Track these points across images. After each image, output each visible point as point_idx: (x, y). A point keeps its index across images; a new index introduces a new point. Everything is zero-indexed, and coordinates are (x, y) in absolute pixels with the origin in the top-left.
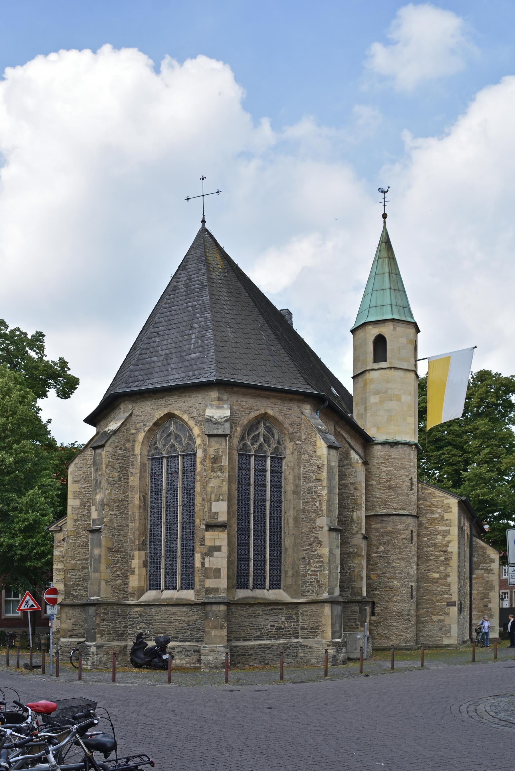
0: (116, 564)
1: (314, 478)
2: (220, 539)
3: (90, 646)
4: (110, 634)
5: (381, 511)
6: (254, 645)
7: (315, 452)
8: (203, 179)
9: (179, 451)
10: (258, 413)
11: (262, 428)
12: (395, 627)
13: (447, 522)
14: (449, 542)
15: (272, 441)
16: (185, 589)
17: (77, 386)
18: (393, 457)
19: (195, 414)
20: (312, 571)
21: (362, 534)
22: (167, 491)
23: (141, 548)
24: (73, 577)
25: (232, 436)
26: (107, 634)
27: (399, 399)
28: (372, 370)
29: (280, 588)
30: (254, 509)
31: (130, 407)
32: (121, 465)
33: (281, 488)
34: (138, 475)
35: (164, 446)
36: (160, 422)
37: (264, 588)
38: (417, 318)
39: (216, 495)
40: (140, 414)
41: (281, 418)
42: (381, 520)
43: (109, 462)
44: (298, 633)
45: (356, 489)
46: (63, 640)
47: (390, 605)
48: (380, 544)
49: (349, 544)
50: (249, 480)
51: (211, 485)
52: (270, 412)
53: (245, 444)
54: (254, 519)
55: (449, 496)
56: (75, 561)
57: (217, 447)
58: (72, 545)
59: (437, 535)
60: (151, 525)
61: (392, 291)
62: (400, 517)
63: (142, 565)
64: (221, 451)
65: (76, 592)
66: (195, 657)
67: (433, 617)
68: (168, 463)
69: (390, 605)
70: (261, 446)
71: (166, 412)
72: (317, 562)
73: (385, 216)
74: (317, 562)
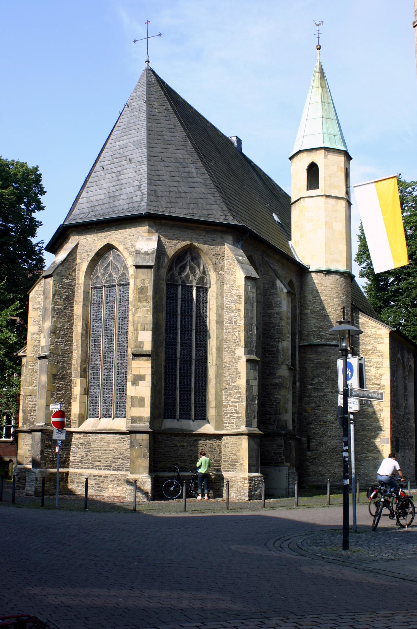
1: (234, 308)
2: (144, 367)
5: (315, 341)
7: (235, 282)
8: (148, 23)
12: (329, 463)
13: (380, 353)
15: (197, 271)
16: (119, 417)
17: (37, 215)
18: (325, 285)
19: (129, 246)
21: (287, 365)
23: (83, 375)
24: (30, 403)
25: (160, 267)
28: (306, 197)
30: (181, 338)
31: (77, 237)
32: (67, 294)
34: (82, 303)
35: (104, 275)
36: (101, 252)
37: (190, 419)
40: (85, 244)
42: (315, 350)
43: (56, 290)
45: (281, 319)
47: (325, 440)
48: (315, 376)
49: (275, 375)
50: (177, 310)
51: (138, 315)
53: (173, 275)
54: (181, 348)
55: (381, 327)
56: (31, 388)
57: (143, 278)
58: (31, 371)
59: (370, 366)
61: (324, 119)
62: (333, 348)
63: (83, 392)
64: (147, 281)
67: (369, 454)
69: (325, 440)
71: (106, 243)
74: (237, 393)
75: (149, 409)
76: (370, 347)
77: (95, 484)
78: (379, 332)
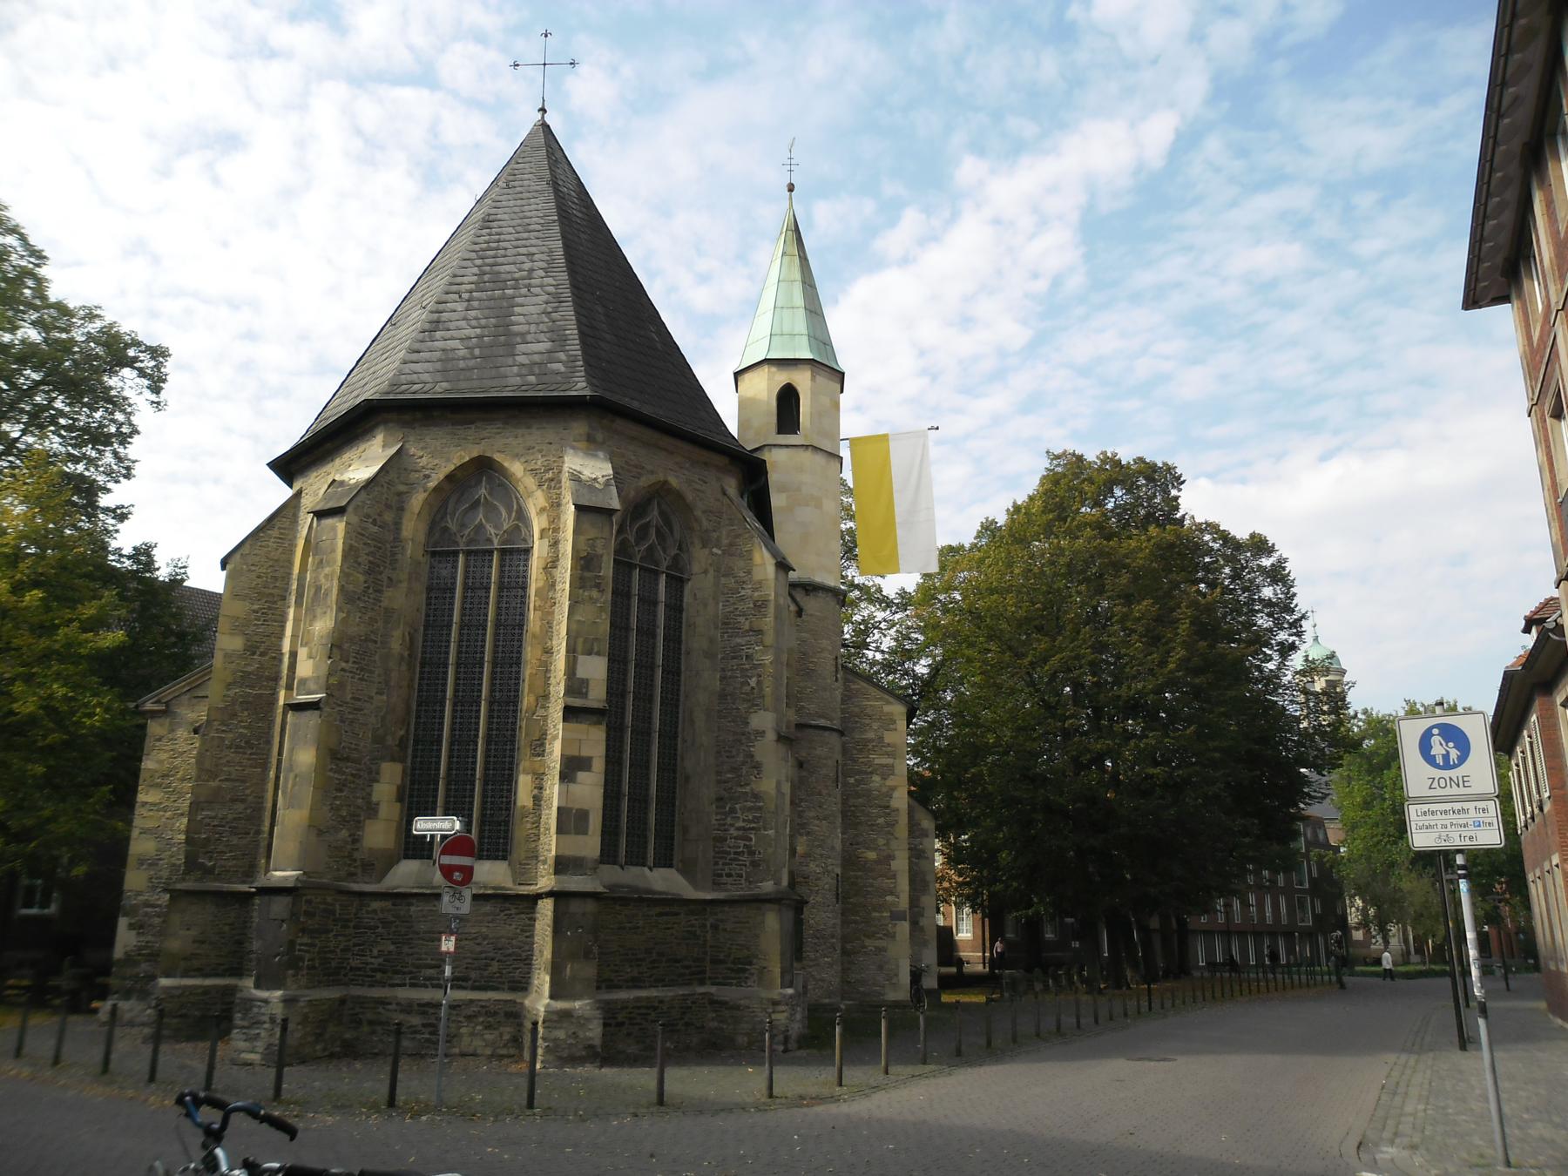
0: (341, 791)
3: (266, 1001)
4: (314, 967)
6: (628, 1001)
7: (749, 572)
9: (496, 541)
10: (653, 479)
11: (654, 515)
14: (893, 789)
20: (738, 829)
22: (461, 628)
26: (309, 968)
27: (819, 506)
29: (671, 866)
33: (680, 643)
38: (843, 364)
39: (586, 640)
41: (690, 497)
43: (351, 547)
44: (704, 972)
46: (164, 982)
52: (674, 481)
60: (419, 705)
64: (600, 543)
65: (211, 859)
66: (507, 1032)
67: (868, 942)
68: (467, 566)
70: (651, 549)
71: (475, 454)
72: (750, 809)
73: (791, 188)
74: (750, 809)
75: (599, 839)
76: (871, 735)
77: (424, 1025)
78: (887, 709)
